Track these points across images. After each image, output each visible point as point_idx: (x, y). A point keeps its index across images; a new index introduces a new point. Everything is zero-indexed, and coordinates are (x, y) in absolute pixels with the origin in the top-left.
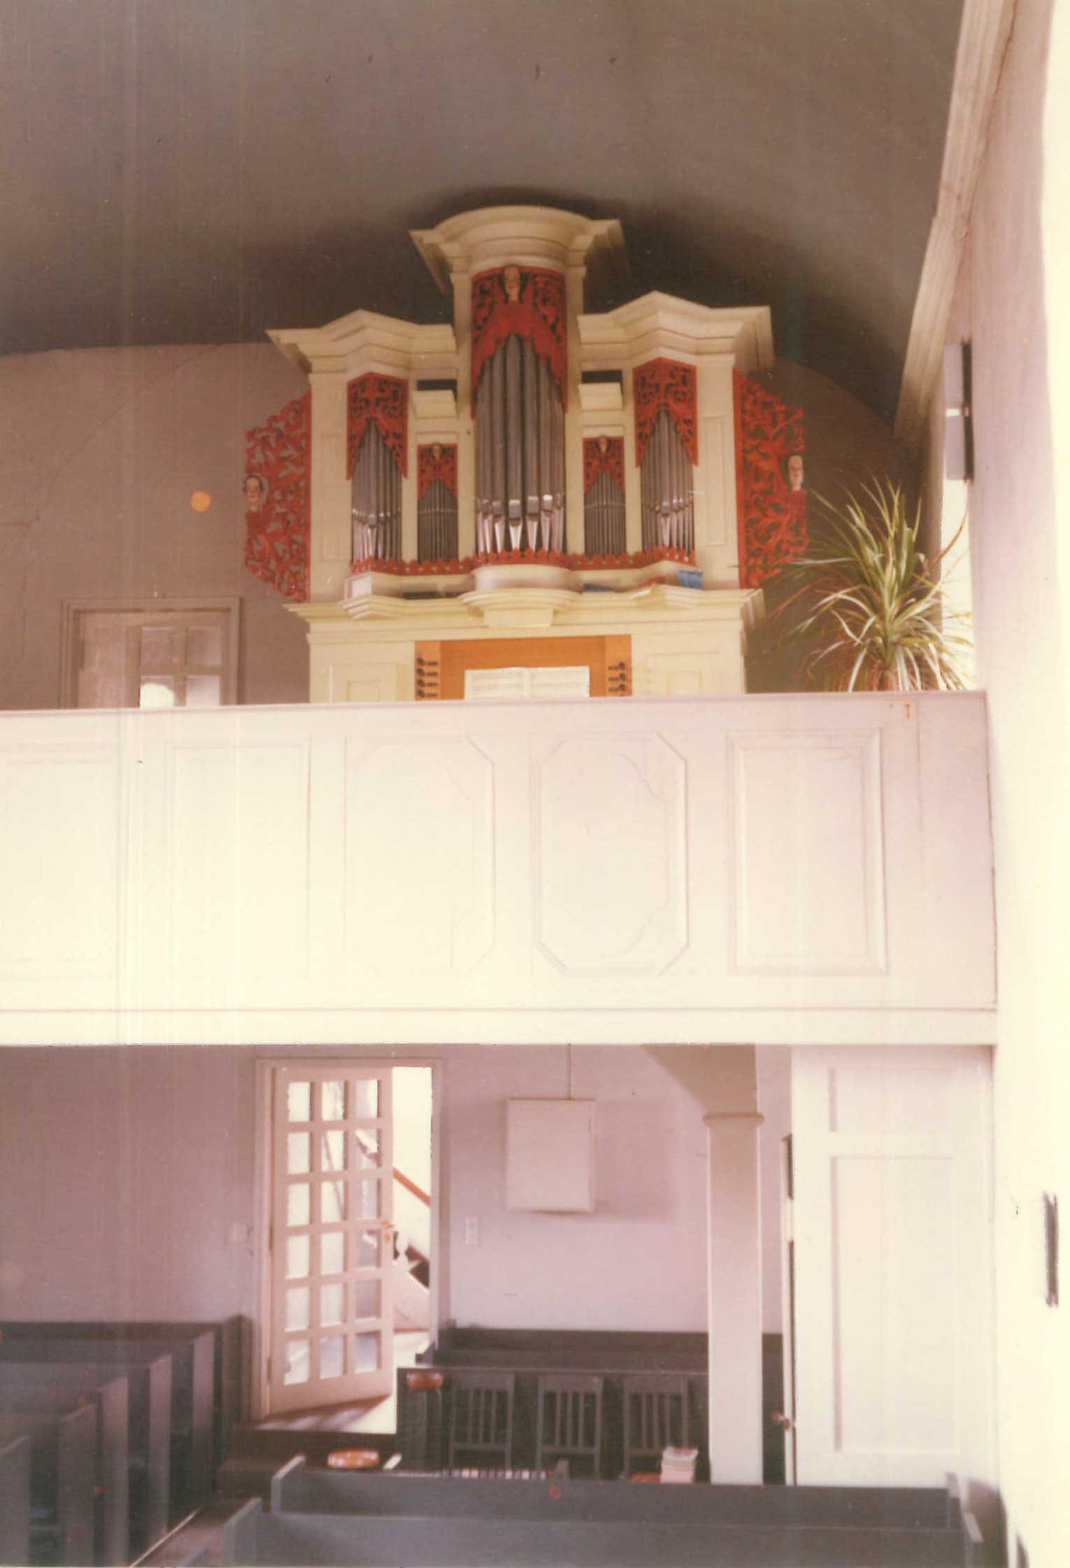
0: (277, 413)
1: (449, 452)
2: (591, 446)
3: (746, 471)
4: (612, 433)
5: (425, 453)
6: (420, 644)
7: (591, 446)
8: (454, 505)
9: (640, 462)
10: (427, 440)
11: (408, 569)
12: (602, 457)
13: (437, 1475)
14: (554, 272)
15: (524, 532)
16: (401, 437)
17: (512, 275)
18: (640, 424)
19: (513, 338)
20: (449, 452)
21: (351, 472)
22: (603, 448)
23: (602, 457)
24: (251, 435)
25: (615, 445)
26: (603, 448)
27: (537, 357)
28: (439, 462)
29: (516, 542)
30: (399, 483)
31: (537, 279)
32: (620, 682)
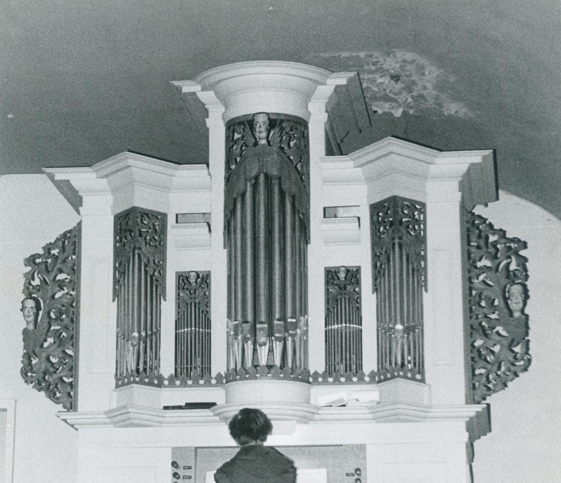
0: (48, 320)
1: (204, 279)
2: (331, 275)
3: (472, 301)
4: (351, 263)
5: (183, 279)
6: (175, 450)
7: (331, 275)
8: (208, 324)
9: (376, 289)
10: (185, 268)
11: (166, 383)
12: (343, 285)
13: (232, 224)
14: (298, 118)
15: (271, 351)
16: (161, 267)
17: (261, 120)
18: (375, 257)
19: (262, 175)
20: (204, 279)
21: (116, 294)
22: (342, 275)
23: (343, 285)
24: (31, 260)
25: (353, 275)
26: (342, 275)
27: (282, 193)
28: (194, 287)
29: (263, 360)
30: (159, 304)
31: (284, 125)
32: (356, 477)
